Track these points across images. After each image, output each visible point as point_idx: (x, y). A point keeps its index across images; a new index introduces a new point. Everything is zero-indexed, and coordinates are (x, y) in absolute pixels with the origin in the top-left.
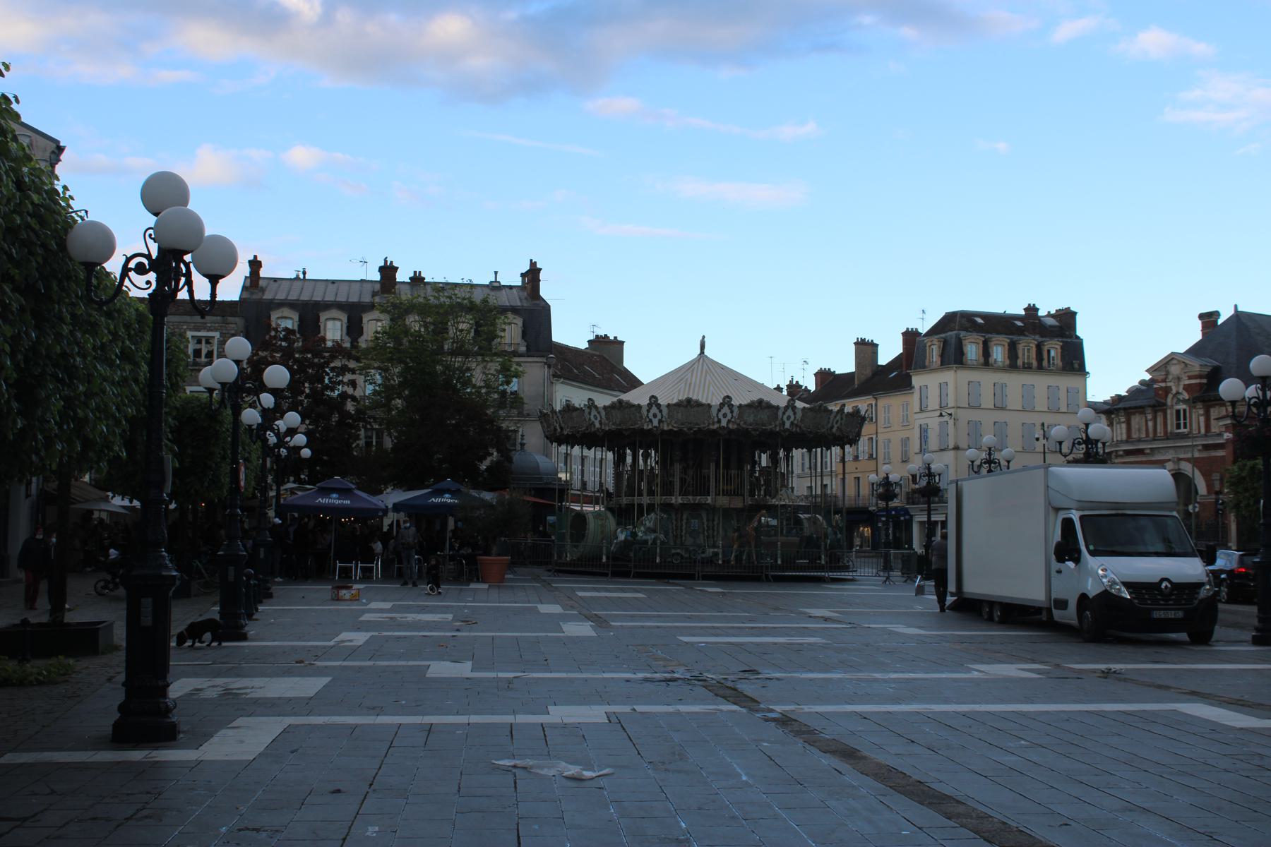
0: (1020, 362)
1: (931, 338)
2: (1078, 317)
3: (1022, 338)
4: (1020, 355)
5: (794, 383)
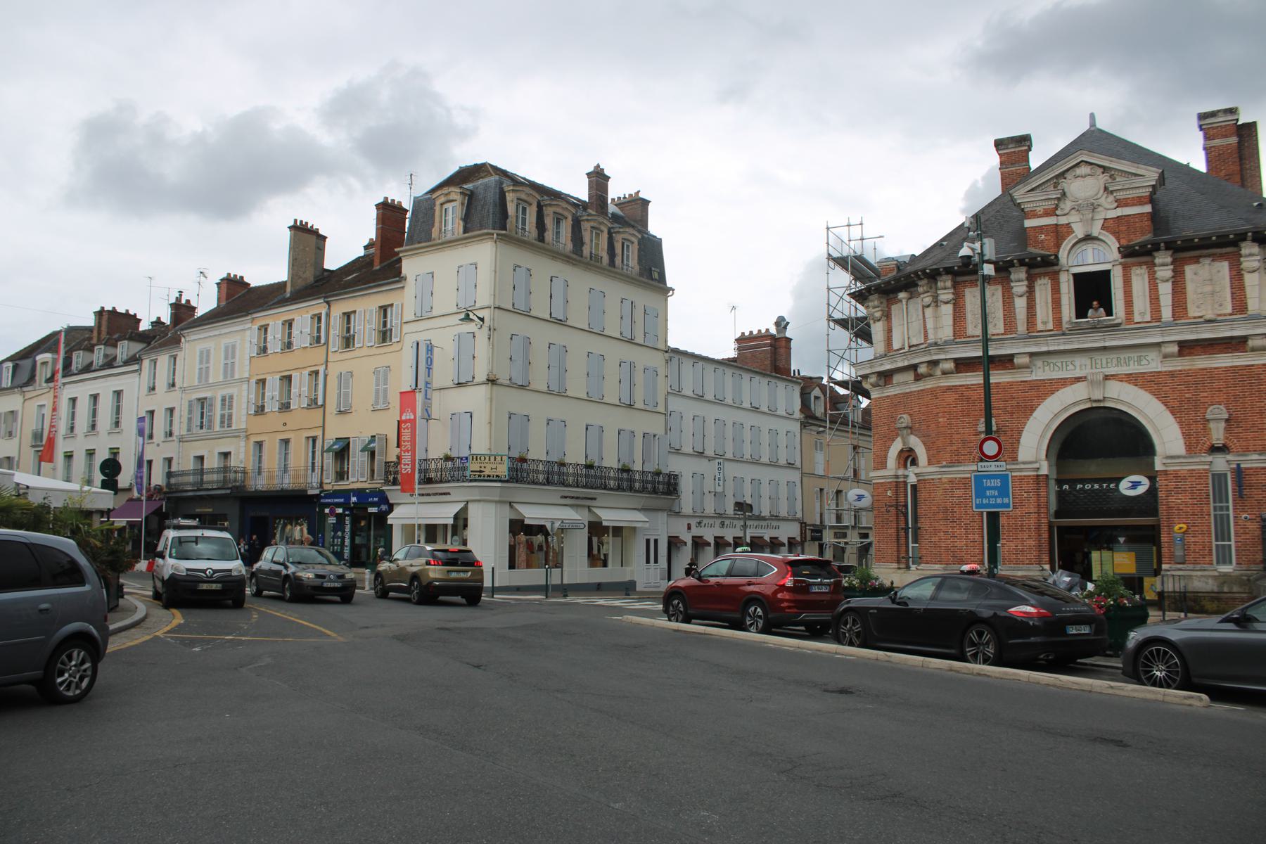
0: (586, 251)
2: (651, 209)
5: (183, 302)
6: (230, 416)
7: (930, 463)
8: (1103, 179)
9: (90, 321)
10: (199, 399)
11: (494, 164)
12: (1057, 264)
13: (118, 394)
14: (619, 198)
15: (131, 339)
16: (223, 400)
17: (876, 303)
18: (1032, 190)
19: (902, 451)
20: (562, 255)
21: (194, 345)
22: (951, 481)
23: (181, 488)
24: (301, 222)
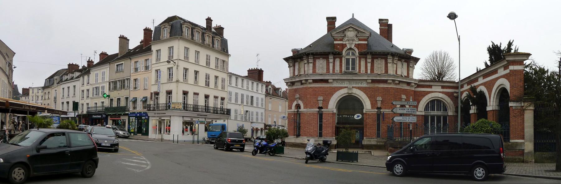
2: (224, 30)
7: (304, 108)
8: (356, 32)
9: (67, 67)
10: (95, 87)
11: (178, 16)
12: (342, 55)
13: (74, 86)
14: (215, 27)
15: (77, 71)
16: (102, 87)
17: (291, 62)
18: (337, 33)
19: (296, 105)
20: (198, 44)
21: (94, 73)
22: (310, 113)
23: (91, 111)
24: (122, 35)
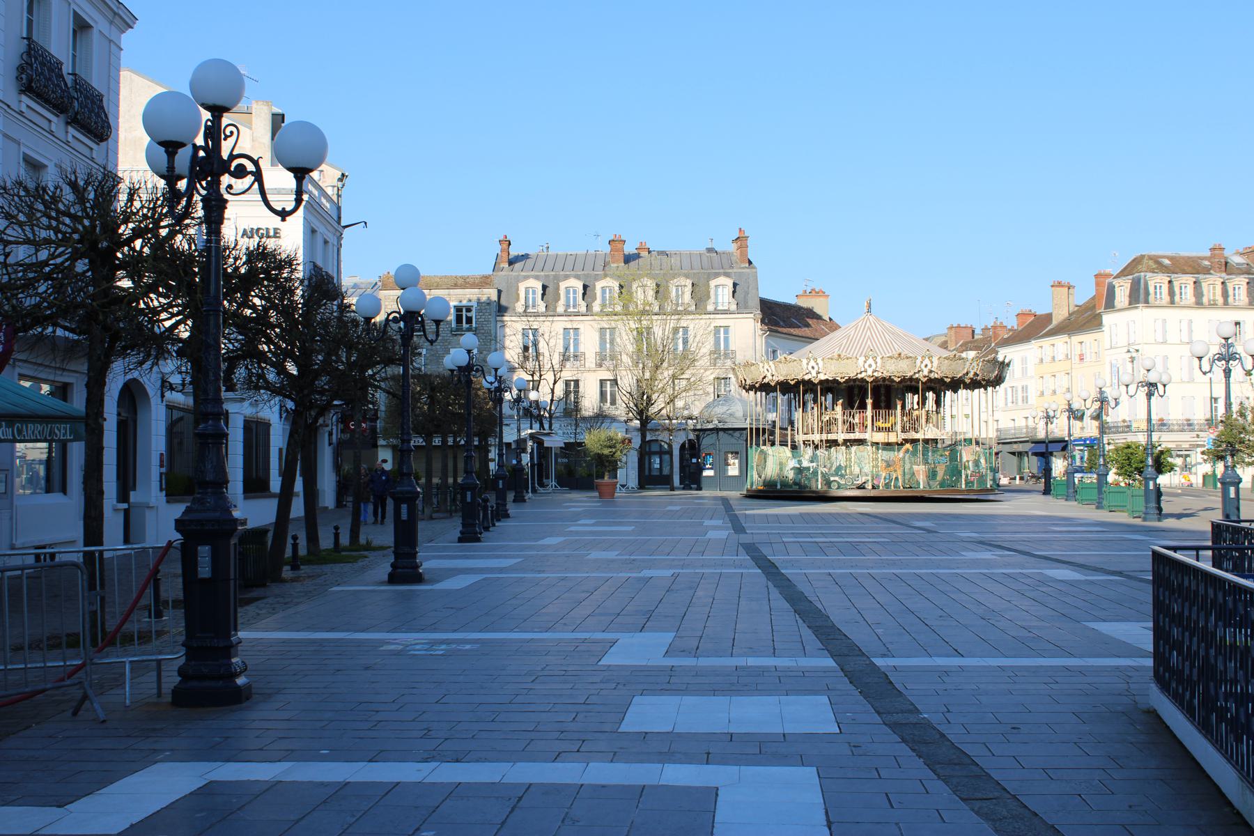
0: (1205, 300)
1: (1119, 280)
3: (1207, 276)
4: (1205, 292)
6: (1027, 397)
